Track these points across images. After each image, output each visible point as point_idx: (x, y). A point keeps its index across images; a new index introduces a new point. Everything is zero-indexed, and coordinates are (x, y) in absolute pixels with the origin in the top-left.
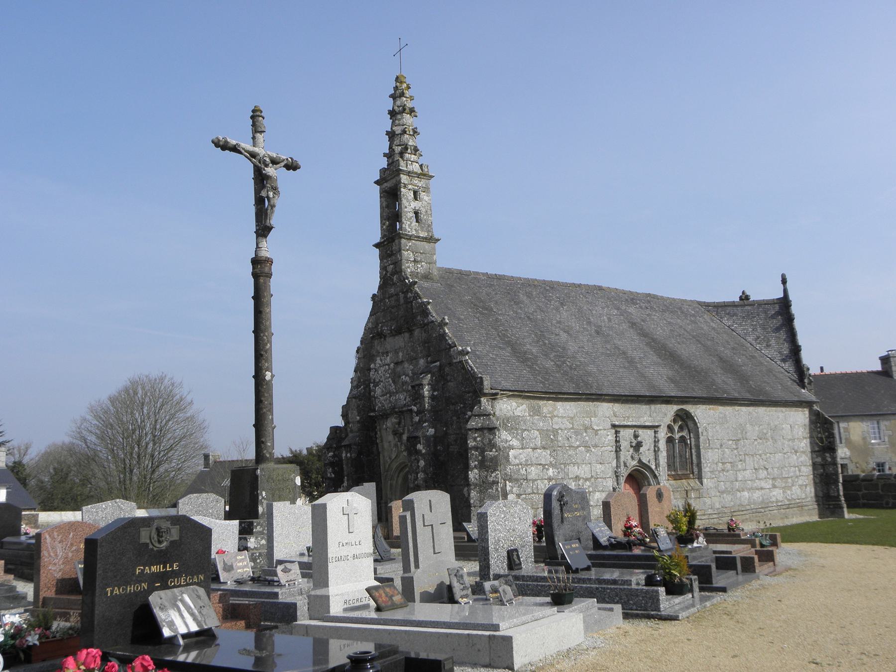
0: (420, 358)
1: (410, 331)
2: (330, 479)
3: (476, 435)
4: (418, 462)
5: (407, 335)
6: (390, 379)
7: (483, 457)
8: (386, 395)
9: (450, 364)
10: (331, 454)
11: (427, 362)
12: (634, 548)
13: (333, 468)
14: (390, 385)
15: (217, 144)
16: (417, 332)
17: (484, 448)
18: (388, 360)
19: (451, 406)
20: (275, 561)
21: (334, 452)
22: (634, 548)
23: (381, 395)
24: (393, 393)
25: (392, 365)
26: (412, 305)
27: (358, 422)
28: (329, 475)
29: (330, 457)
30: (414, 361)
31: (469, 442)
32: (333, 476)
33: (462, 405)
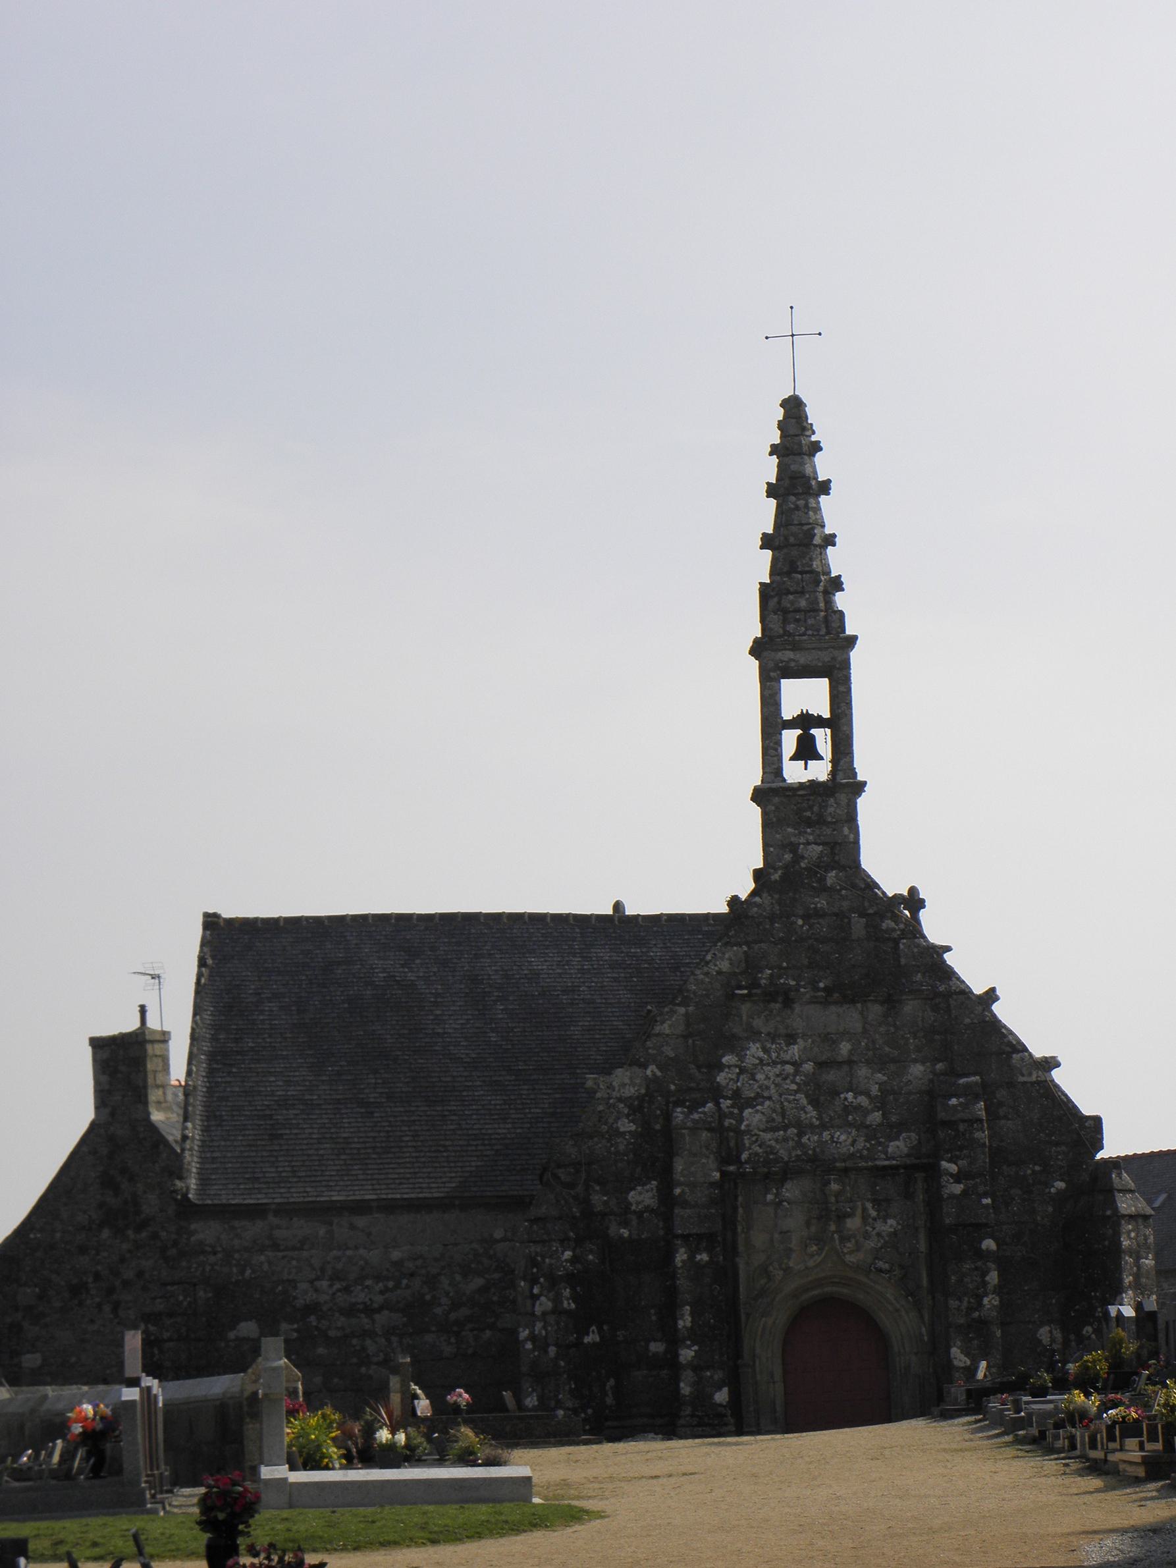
0: (915, 1061)
1: (891, 1003)
2: (568, 1312)
3: (1130, 1227)
4: (984, 1274)
5: (876, 1010)
6: (798, 1096)
7: (1139, 1267)
8: (785, 1128)
9: (1011, 1084)
10: (568, 1254)
11: (933, 1072)
12: (1139, 1460)
13: (573, 1289)
14: (803, 1109)
15: (794, 409)
16: (910, 1007)
17: (1138, 1252)
18: (795, 1051)
19: (1005, 1167)
20: (1161, 1441)
21: (573, 1250)
22: (1139, 1460)
23: (762, 1127)
24: (812, 1126)
25: (808, 1067)
26: (896, 947)
27: (713, 1184)
28: (565, 1304)
29: (566, 1261)
30: (892, 1067)
31: (1122, 1239)
32: (573, 1306)
33: (1037, 1168)
